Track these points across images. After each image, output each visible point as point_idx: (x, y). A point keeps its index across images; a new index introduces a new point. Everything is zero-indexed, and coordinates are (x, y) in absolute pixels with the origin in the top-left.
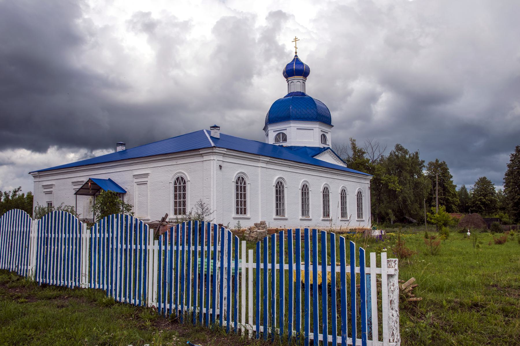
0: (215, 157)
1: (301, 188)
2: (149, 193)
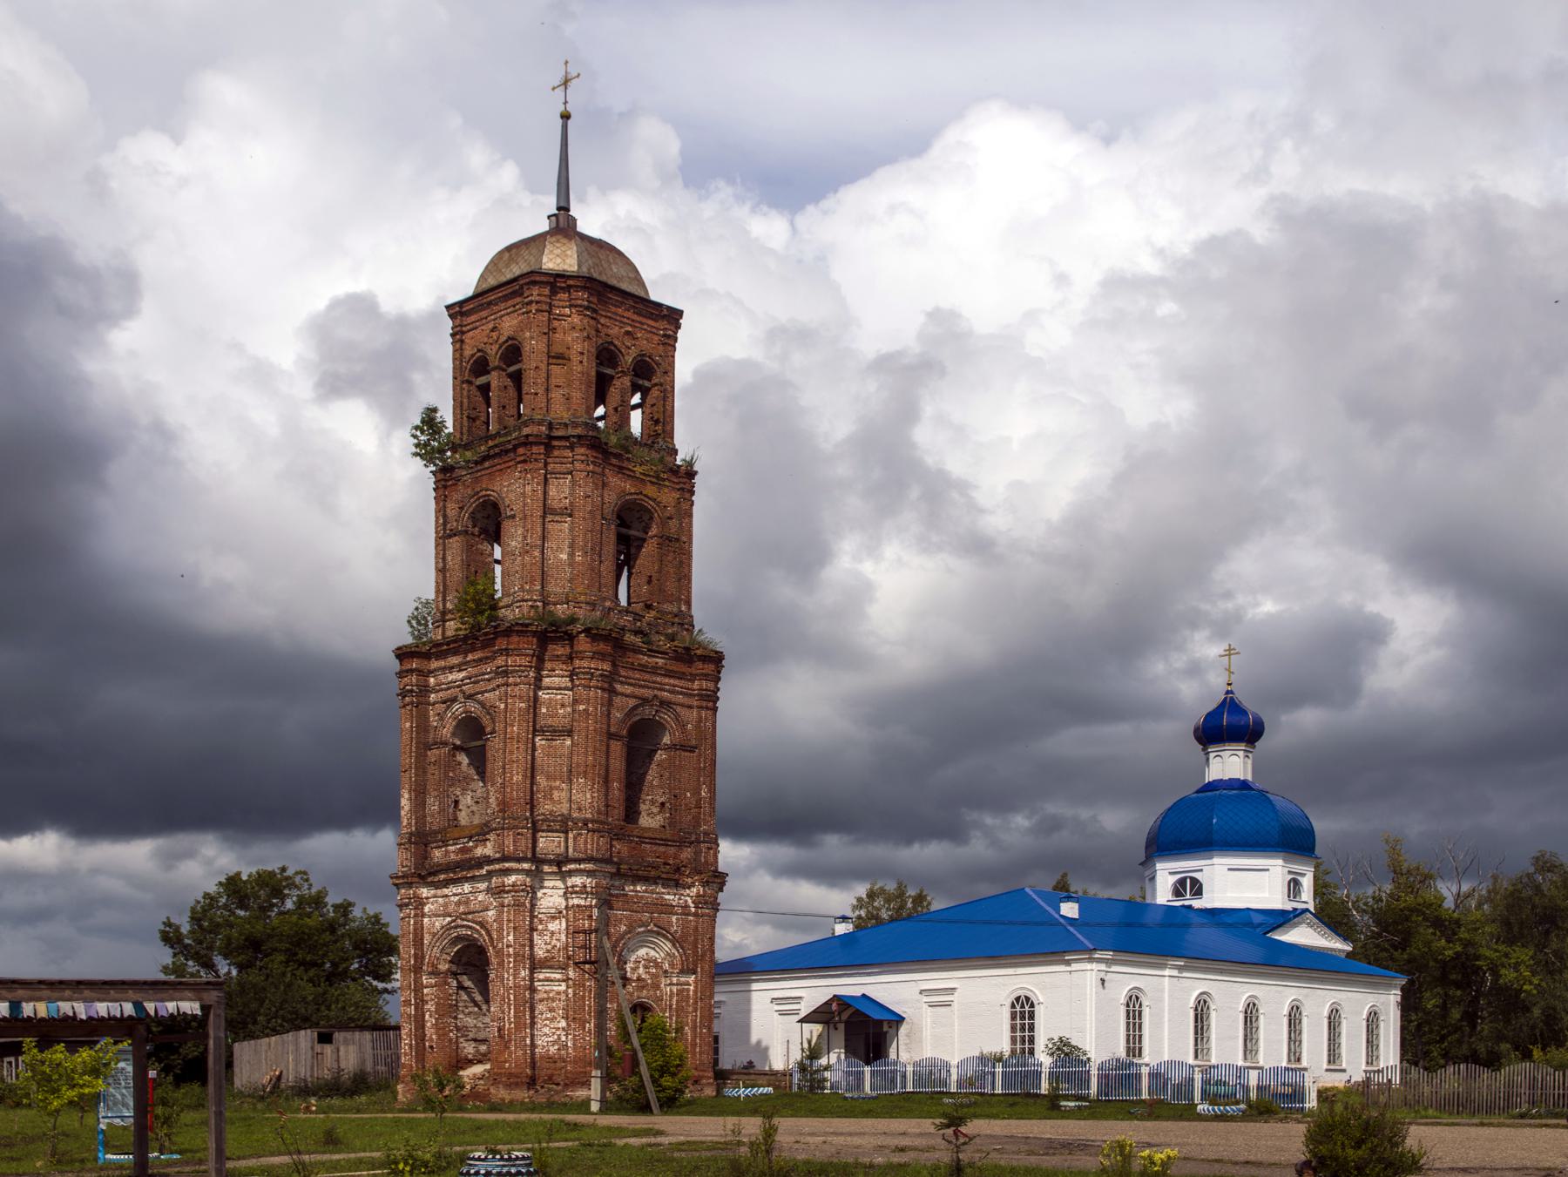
0: (1094, 966)
1: (1244, 1010)
2: (956, 1020)
